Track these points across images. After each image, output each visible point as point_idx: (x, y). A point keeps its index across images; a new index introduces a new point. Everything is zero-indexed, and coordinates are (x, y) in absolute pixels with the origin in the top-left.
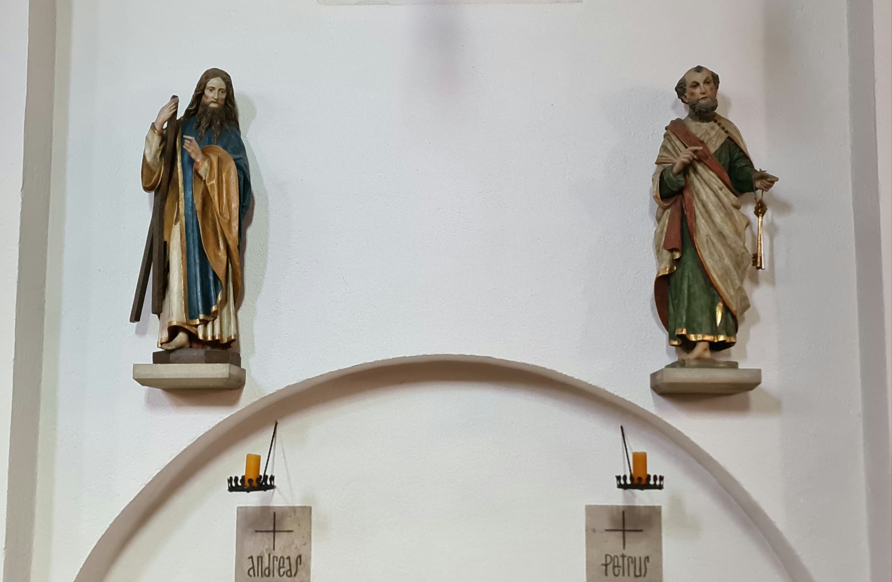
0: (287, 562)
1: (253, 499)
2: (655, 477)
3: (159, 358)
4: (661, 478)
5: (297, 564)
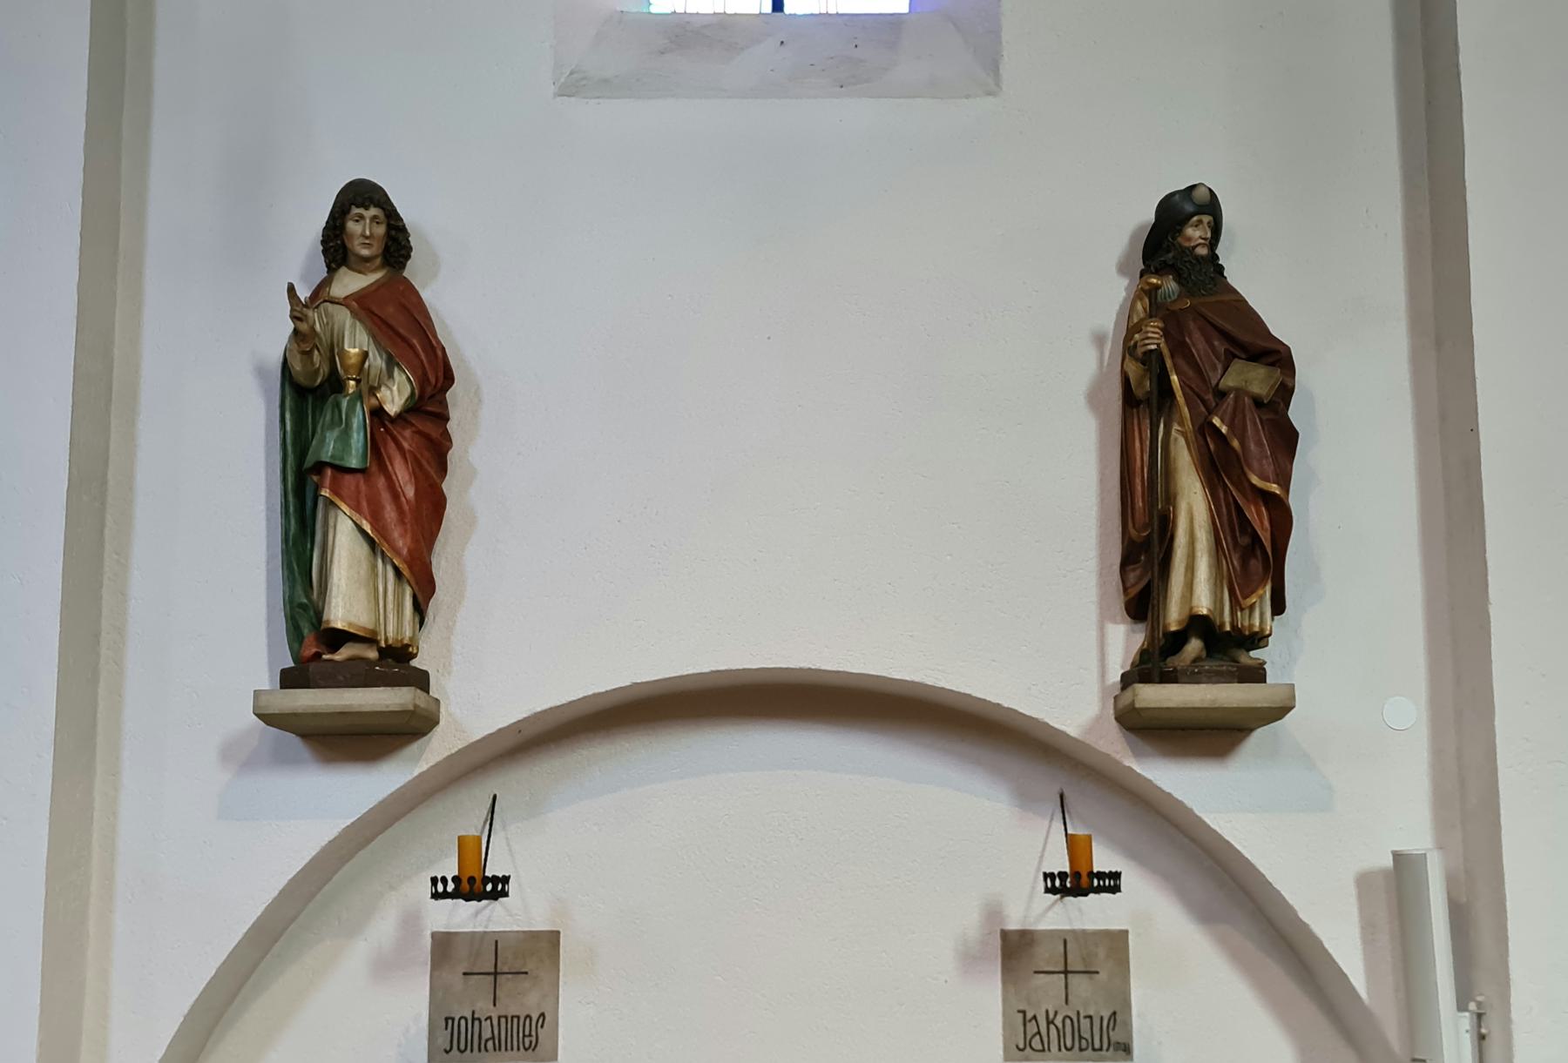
0: (1085, 1023)
1: (462, 916)
3: (290, 680)
5: (531, 1031)
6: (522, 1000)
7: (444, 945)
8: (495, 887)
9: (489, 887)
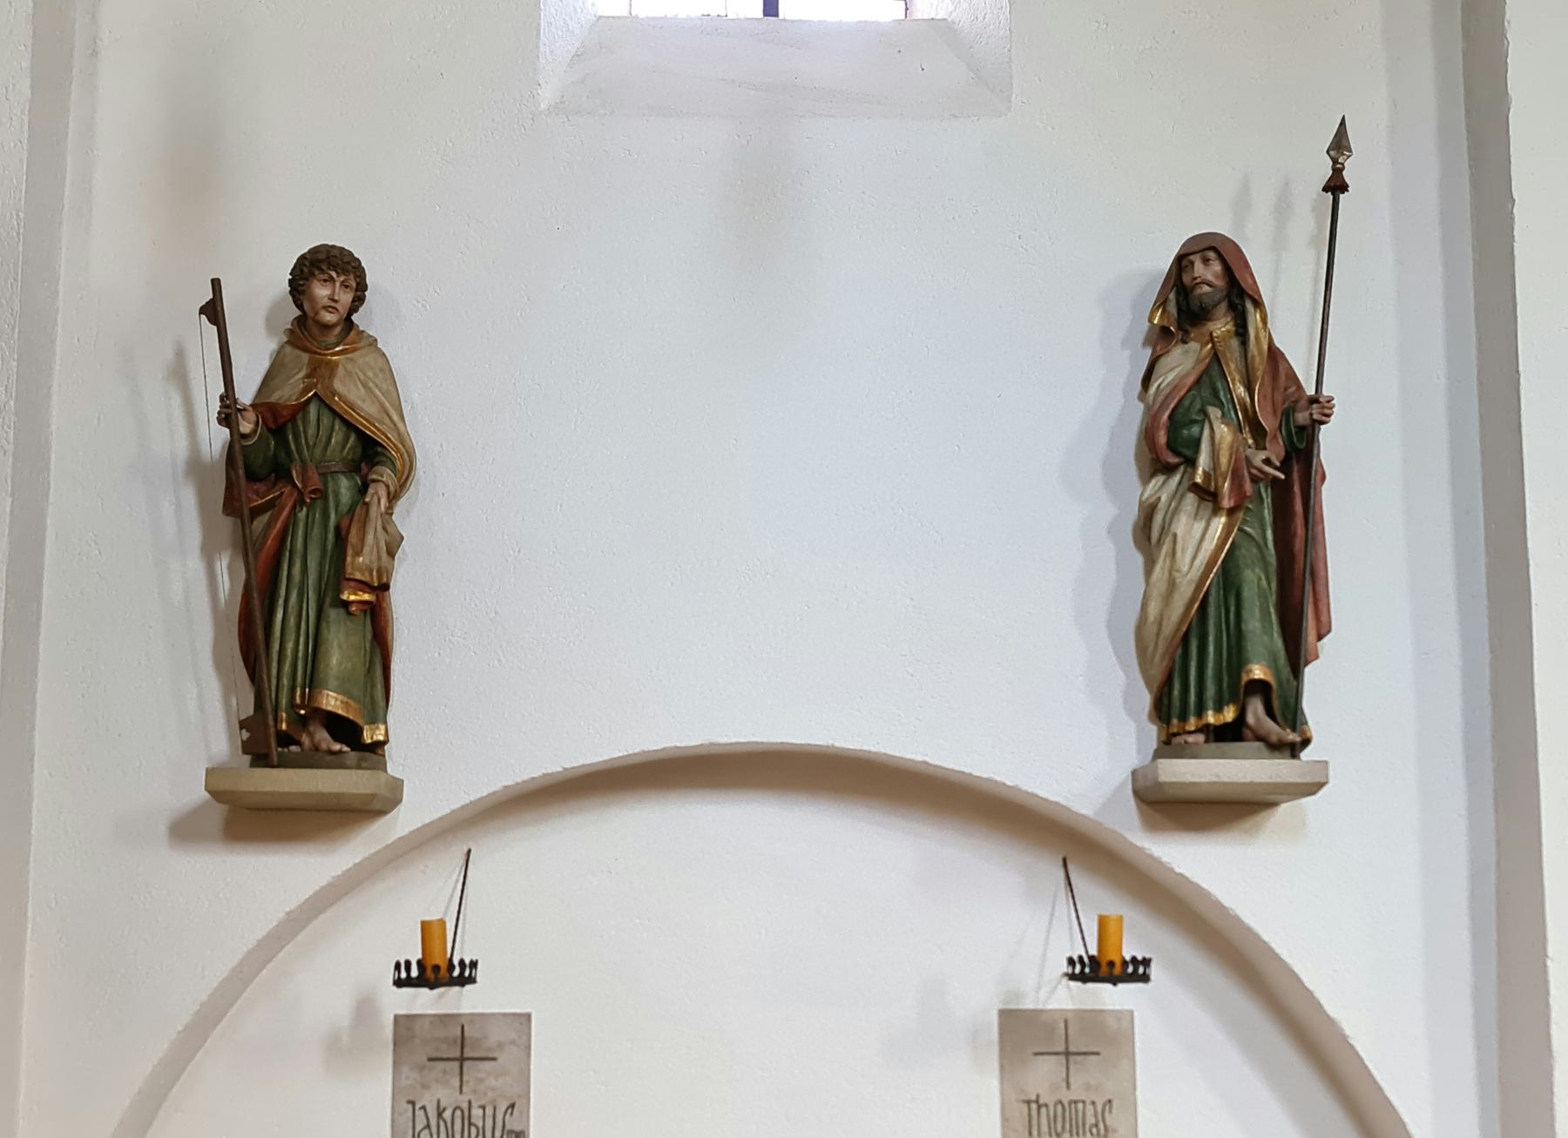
1: (424, 1001)
2: (462, 963)
4: (474, 964)
6: (487, 1081)
7: (405, 1025)
8: (1136, 970)
9: (1130, 969)
